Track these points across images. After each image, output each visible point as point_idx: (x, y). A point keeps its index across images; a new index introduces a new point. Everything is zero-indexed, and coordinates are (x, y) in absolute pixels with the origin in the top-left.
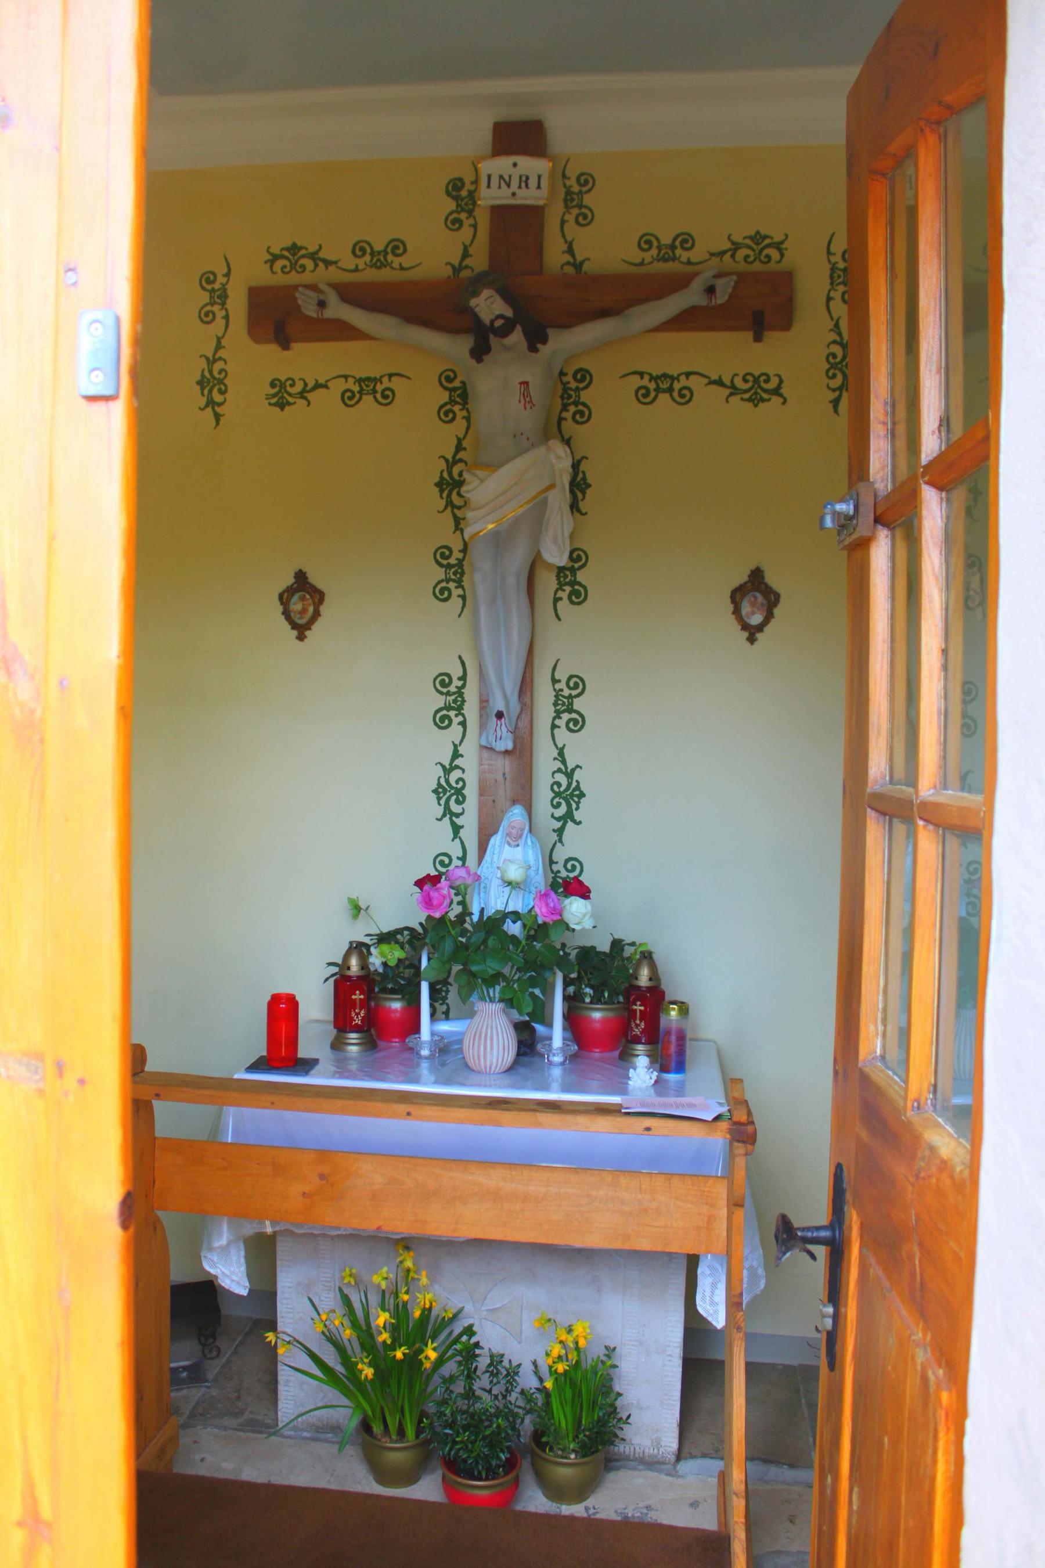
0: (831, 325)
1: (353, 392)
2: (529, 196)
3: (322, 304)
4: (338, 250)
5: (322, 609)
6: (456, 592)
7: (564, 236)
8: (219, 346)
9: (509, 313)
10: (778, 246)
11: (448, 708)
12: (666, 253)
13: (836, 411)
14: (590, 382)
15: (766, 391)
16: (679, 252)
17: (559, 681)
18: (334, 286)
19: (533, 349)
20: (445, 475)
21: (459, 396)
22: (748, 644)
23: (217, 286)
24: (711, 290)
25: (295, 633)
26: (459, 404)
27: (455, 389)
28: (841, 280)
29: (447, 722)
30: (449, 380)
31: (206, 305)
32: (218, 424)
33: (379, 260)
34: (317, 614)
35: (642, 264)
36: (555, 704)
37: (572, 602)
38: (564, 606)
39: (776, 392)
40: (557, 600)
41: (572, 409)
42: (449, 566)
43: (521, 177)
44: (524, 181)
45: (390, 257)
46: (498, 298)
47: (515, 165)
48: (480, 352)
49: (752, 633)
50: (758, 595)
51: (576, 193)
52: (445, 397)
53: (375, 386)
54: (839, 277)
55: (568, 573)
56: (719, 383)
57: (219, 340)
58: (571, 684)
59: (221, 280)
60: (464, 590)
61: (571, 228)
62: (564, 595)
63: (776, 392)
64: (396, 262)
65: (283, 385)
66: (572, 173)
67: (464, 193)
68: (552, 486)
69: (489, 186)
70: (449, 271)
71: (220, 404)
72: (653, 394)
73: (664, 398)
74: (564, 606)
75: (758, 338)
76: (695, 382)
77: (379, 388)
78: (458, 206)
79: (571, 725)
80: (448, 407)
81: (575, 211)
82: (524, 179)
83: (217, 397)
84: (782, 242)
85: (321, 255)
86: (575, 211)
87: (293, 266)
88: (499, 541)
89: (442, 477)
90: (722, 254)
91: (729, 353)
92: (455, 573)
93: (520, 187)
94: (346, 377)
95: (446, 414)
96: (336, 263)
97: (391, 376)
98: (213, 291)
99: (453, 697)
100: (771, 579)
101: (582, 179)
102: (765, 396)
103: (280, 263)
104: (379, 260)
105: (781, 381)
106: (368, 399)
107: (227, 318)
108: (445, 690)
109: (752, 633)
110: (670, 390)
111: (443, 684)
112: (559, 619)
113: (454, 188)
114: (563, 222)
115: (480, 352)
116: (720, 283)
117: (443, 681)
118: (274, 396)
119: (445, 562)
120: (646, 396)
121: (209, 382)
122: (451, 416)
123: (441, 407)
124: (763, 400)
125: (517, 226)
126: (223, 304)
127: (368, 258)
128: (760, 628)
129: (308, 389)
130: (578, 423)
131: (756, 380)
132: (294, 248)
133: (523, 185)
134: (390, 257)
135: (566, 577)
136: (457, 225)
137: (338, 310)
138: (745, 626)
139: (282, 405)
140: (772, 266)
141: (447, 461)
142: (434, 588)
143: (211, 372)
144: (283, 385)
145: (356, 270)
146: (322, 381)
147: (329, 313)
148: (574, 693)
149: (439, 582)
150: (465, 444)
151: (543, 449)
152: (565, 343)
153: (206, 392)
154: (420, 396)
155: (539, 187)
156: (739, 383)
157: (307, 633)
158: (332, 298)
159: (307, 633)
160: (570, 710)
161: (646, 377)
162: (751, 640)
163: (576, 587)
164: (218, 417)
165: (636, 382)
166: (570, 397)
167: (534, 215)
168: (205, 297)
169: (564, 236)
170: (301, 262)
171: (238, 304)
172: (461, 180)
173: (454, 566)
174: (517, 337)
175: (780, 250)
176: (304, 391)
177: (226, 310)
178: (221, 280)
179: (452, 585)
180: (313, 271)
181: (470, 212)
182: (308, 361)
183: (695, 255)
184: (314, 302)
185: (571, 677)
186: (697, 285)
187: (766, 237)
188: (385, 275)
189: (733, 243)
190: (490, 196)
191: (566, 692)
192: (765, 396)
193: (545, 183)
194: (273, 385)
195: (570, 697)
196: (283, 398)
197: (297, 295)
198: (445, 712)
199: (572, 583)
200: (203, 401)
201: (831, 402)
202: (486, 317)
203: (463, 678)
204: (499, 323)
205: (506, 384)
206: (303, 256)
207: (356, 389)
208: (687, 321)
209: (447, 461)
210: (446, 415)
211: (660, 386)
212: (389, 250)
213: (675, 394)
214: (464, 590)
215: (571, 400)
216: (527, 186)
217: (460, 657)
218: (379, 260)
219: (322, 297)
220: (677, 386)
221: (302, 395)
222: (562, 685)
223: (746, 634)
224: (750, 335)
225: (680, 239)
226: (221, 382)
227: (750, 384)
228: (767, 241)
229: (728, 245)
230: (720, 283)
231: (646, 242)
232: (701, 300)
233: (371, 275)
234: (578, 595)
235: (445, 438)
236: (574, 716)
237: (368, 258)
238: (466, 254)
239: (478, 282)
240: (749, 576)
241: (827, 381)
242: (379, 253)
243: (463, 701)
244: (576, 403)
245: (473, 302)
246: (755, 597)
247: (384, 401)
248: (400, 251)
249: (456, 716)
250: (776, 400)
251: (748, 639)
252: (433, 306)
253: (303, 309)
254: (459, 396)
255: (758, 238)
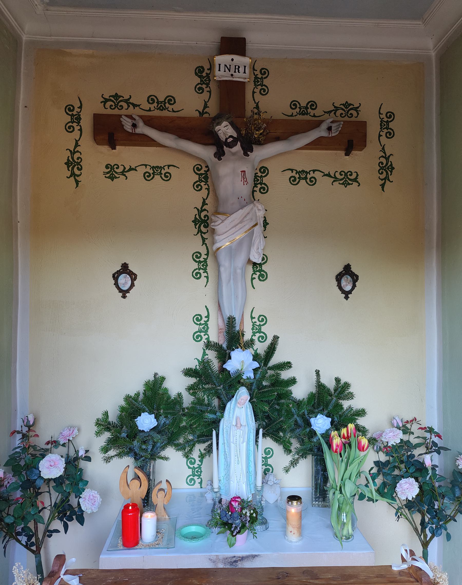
0: (381, 148)
1: (149, 173)
2: (239, 77)
3: (134, 126)
4: (140, 98)
5: (135, 282)
6: (204, 275)
7: (254, 100)
8: (77, 145)
9: (235, 135)
10: (356, 109)
11: (200, 331)
12: (303, 111)
13: (383, 190)
14: (268, 173)
15: (350, 180)
16: (309, 110)
17: (255, 318)
18: (141, 117)
19: (246, 154)
20: (197, 217)
21: (204, 176)
22: (345, 300)
23: (75, 113)
24: (329, 129)
25: (121, 294)
26: (204, 182)
27: (201, 174)
28: (385, 127)
29: (200, 338)
30: (199, 170)
31: (69, 122)
32: (77, 186)
33: (161, 106)
34: (132, 285)
35: (292, 116)
36: (253, 329)
37: (260, 280)
38: (256, 281)
39: (355, 180)
40: (253, 279)
41: (259, 186)
42: (200, 262)
43: (235, 66)
44: (237, 68)
45: (167, 105)
46: (230, 127)
47: (232, 60)
48: (219, 155)
49: (347, 294)
50: (348, 277)
51: (260, 77)
52: (196, 178)
53: (161, 171)
54: (385, 125)
55: (258, 266)
56: (329, 175)
57: (77, 141)
58: (260, 320)
59: (77, 110)
60: (207, 274)
61: (257, 95)
62: (256, 276)
63: (355, 180)
64: (171, 107)
65: (112, 168)
66: (258, 67)
67: (204, 74)
68: (256, 225)
69: (219, 70)
70: (197, 114)
71: (78, 176)
72: (298, 180)
73: (303, 182)
74: (256, 281)
75: (347, 154)
76: (317, 175)
77: (163, 172)
78: (201, 81)
79: (260, 339)
80: (199, 183)
81: (260, 87)
82: (237, 67)
83: (77, 172)
84: (358, 107)
85: (131, 101)
86: (260, 87)
87: (116, 106)
88: (232, 252)
89: (195, 218)
90: (330, 112)
91: (333, 160)
92: (203, 266)
93: (235, 72)
94: (146, 165)
95: (197, 186)
96: (139, 106)
97: (169, 166)
98: (72, 115)
99: (203, 326)
100: (354, 269)
101: (263, 71)
102: (350, 182)
103: (109, 104)
104: (161, 106)
105: (357, 175)
106: (157, 177)
107: (81, 130)
108: (199, 323)
109: (347, 294)
110: (306, 178)
111: (197, 319)
112: (254, 288)
113: (199, 71)
114: (254, 92)
115: (219, 155)
116: (334, 125)
117: (198, 318)
118: (108, 173)
119: (198, 260)
120: (294, 181)
121: (72, 163)
122: (200, 187)
123: (195, 183)
124: (349, 184)
125: (232, 92)
126: (79, 123)
127: (155, 104)
128: (350, 292)
129: (126, 170)
130: (262, 193)
131: (346, 174)
132: (116, 96)
133: (237, 70)
134: (167, 105)
135: (257, 267)
136: (201, 91)
137: (142, 129)
138: (343, 291)
139: (112, 178)
140: (353, 119)
141: (198, 210)
142: (193, 272)
143: (73, 158)
144: (112, 168)
145: (150, 110)
146: (133, 167)
147: (138, 131)
148: (262, 323)
149: (195, 270)
150: (207, 202)
151: (252, 205)
152: (261, 153)
153: (70, 169)
154: (185, 176)
155: (245, 72)
156: (338, 175)
157: (127, 295)
158: (141, 124)
159: (127, 295)
160: (260, 332)
161: (295, 172)
162: (347, 298)
163: (262, 273)
164: (77, 182)
165: (289, 174)
166: (258, 180)
167: (240, 86)
168: (69, 119)
169: (254, 100)
170: (120, 104)
171: (87, 122)
172: (202, 67)
173: (202, 262)
174: (238, 148)
175: (357, 111)
176: (124, 171)
177: (80, 126)
178: (77, 110)
179: (201, 271)
180: (127, 109)
181: (208, 85)
182: (126, 155)
183: (318, 112)
184: (130, 124)
185: (260, 316)
186: (324, 126)
187: (351, 104)
188: (165, 113)
189: (335, 107)
190: (221, 75)
191: (258, 323)
192: (350, 182)
193: (247, 71)
194: (107, 167)
195: (260, 325)
196: (112, 174)
197: (121, 119)
198: (199, 333)
199: (260, 271)
200: (69, 173)
201: (380, 185)
202: (223, 138)
203: (208, 317)
204: (230, 140)
205: (232, 174)
206: (121, 101)
207: (151, 172)
208: (316, 144)
209: (198, 210)
210: (197, 187)
211: (300, 177)
212: (167, 101)
213: (308, 180)
214: (207, 274)
215: (259, 182)
216: (239, 72)
217: (206, 306)
218: (161, 106)
219: (134, 122)
220: (309, 176)
221: (123, 173)
222: (256, 320)
223: (344, 295)
224: (343, 153)
225: (310, 104)
226: (78, 164)
227: (343, 176)
228: (351, 107)
229: (333, 108)
230: (334, 125)
231: (294, 105)
232: (324, 134)
233: (157, 113)
234: (263, 277)
235: (196, 199)
236: (262, 334)
237: (155, 104)
238: (206, 106)
239: (217, 119)
240: (344, 268)
241: (379, 175)
242: (161, 102)
243: (208, 328)
244: (261, 184)
245: (217, 128)
246: (347, 278)
247: (166, 179)
248: (172, 102)
249: (204, 335)
250: (355, 184)
251: (345, 298)
252: (200, 131)
253: (124, 127)
254: (204, 176)
255: (347, 105)
